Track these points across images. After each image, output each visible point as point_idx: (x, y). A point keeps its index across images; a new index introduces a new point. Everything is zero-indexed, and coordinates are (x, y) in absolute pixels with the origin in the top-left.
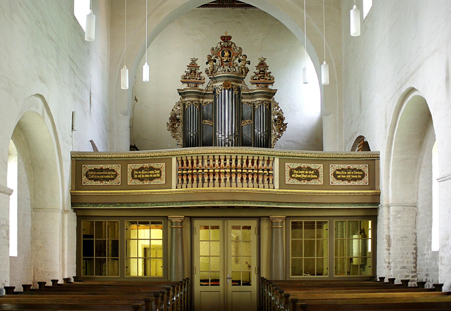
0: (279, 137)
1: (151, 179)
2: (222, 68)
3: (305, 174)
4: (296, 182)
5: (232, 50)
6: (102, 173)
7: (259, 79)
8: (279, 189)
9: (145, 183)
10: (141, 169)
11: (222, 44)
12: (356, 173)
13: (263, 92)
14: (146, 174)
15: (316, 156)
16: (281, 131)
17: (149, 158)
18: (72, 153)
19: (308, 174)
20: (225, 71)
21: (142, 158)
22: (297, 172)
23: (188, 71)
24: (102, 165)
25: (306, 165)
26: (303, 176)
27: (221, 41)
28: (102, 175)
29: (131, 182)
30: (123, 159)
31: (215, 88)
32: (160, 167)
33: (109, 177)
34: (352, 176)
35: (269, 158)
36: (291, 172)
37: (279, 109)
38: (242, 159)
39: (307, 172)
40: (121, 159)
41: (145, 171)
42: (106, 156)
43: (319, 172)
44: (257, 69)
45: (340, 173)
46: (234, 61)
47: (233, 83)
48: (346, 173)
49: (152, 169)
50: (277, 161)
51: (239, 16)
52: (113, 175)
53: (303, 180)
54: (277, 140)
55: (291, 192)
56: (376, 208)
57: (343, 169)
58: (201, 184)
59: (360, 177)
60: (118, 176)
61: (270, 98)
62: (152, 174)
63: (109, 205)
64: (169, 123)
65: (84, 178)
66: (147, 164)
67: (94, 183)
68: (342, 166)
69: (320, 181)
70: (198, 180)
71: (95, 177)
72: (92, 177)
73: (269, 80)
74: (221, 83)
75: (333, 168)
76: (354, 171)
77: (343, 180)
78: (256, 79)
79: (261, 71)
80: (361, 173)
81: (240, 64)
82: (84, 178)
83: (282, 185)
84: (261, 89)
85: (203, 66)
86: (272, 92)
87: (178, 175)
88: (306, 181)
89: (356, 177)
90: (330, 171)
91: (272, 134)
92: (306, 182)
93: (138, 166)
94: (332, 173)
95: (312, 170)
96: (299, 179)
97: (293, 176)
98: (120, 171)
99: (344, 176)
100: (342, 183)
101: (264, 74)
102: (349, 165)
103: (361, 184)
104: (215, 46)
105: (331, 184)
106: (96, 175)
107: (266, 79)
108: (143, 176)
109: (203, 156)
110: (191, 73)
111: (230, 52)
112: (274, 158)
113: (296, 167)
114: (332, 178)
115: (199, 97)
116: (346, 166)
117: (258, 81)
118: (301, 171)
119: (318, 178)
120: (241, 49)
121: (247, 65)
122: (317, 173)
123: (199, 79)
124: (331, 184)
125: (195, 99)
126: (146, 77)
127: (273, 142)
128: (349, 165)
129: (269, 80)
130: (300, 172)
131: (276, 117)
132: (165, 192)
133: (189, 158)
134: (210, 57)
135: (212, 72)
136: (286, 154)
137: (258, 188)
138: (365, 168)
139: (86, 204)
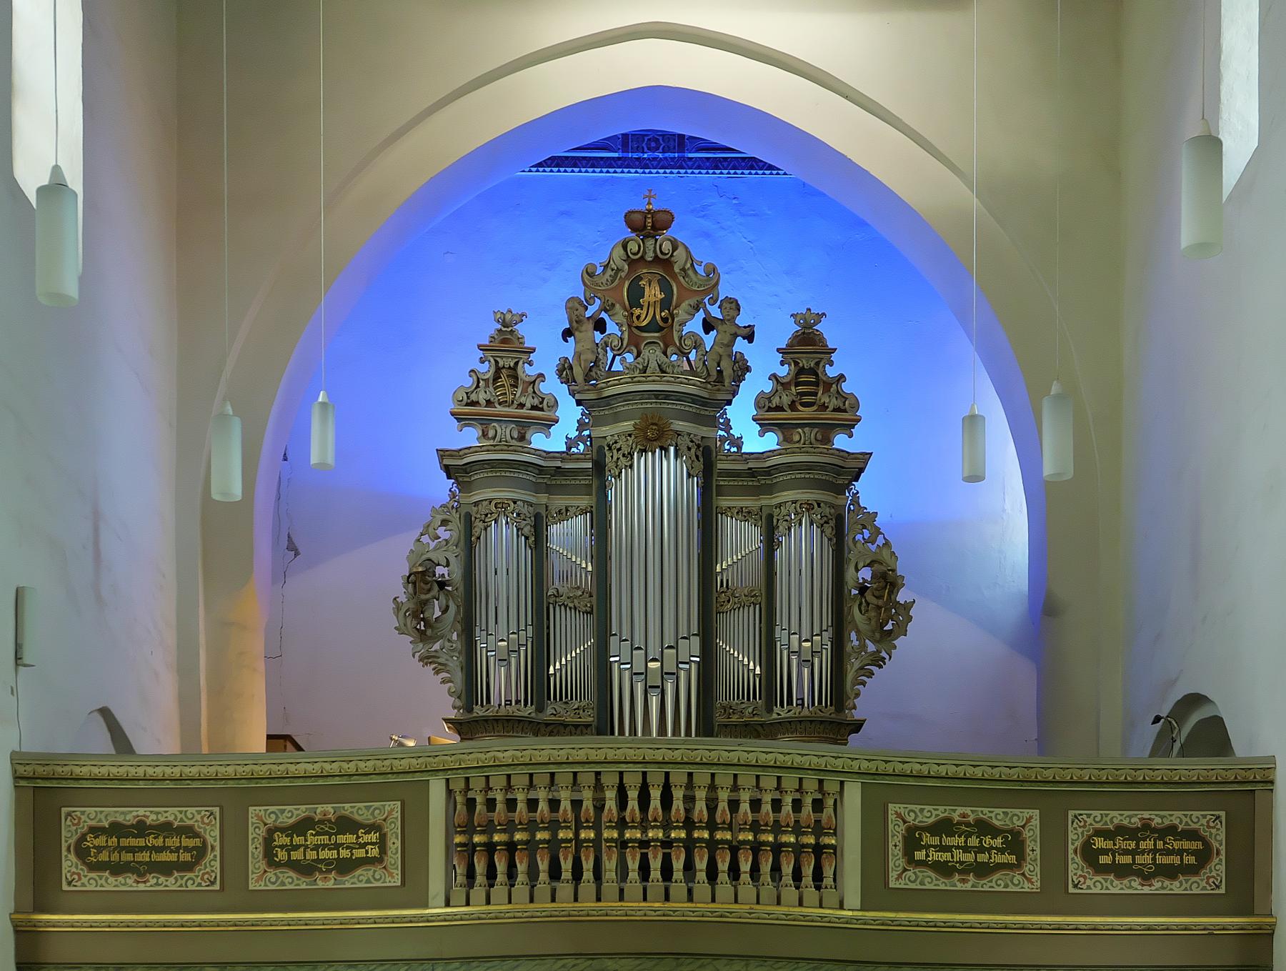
0: (878, 661)
1: (345, 867)
2: (630, 358)
3: (966, 849)
4: (932, 882)
5: (674, 276)
6: (141, 842)
7: (792, 406)
9: (321, 885)
10: (302, 826)
11: (633, 247)
12: (1177, 845)
13: (809, 466)
14: (324, 846)
16: (886, 638)
17: (336, 781)
18: (17, 759)
19: (981, 849)
22: (936, 841)
23: (483, 368)
24: (141, 811)
26: (959, 855)
27: (628, 233)
28: (141, 849)
29: (260, 879)
31: (601, 448)
32: (379, 818)
34: (1161, 860)
36: (912, 842)
37: (880, 541)
38: (713, 787)
39: (973, 841)
40: (220, 785)
41: (318, 834)
42: (158, 770)
43: (1023, 842)
44: (782, 363)
45: (1109, 844)
46: (683, 324)
47: (679, 425)
48: (1133, 845)
49: (346, 825)
51: (704, 208)
52: (187, 849)
54: (871, 674)
57: (1121, 831)
60: (210, 856)
61: (840, 490)
64: (403, 598)
65: (70, 863)
66: (329, 808)
67: (111, 883)
68: (1118, 817)
69: (1029, 880)
72: (104, 857)
74: (627, 426)
75: (1082, 824)
76: (1169, 838)
77: (1121, 872)
78: (779, 408)
79: (801, 371)
80: (1197, 845)
81: (709, 340)
82: (70, 863)
83: (876, 891)
84: (801, 451)
85: (547, 350)
86: (851, 464)
88: (971, 877)
89: (1176, 860)
90: (1071, 836)
91: (848, 648)
92: (971, 883)
93: (291, 814)
94: (1078, 844)
96: (944, 869)
97: (920, 855)
98: (217, 833)
99: (1127, 859)
100: (1116, 887)
102: (1146, 815)
103: (1195, 891)
104: (599, 259)
105: (1071, 890)
106: (120, 849)
107: (824, 407)
108: (311, 855)
110: (496, 377)
111: (665, 287)
112: (842, 783)
113: (931, 820)
114: (1076, 866)
115: (537, 488)
116: (1133, 819)
118: (951, 835)
119: (1018, 866)
122: (1015, 843)
123: (534, 408)
124: (1071, 890)
125: (515, 496)
126: (321, 447)
128: (1146, 815)
130: (948, 841)
131: (866, 574)
135: (587, 378)
136: (889, 768)
137: (779, 903)
138: (1211, 824)
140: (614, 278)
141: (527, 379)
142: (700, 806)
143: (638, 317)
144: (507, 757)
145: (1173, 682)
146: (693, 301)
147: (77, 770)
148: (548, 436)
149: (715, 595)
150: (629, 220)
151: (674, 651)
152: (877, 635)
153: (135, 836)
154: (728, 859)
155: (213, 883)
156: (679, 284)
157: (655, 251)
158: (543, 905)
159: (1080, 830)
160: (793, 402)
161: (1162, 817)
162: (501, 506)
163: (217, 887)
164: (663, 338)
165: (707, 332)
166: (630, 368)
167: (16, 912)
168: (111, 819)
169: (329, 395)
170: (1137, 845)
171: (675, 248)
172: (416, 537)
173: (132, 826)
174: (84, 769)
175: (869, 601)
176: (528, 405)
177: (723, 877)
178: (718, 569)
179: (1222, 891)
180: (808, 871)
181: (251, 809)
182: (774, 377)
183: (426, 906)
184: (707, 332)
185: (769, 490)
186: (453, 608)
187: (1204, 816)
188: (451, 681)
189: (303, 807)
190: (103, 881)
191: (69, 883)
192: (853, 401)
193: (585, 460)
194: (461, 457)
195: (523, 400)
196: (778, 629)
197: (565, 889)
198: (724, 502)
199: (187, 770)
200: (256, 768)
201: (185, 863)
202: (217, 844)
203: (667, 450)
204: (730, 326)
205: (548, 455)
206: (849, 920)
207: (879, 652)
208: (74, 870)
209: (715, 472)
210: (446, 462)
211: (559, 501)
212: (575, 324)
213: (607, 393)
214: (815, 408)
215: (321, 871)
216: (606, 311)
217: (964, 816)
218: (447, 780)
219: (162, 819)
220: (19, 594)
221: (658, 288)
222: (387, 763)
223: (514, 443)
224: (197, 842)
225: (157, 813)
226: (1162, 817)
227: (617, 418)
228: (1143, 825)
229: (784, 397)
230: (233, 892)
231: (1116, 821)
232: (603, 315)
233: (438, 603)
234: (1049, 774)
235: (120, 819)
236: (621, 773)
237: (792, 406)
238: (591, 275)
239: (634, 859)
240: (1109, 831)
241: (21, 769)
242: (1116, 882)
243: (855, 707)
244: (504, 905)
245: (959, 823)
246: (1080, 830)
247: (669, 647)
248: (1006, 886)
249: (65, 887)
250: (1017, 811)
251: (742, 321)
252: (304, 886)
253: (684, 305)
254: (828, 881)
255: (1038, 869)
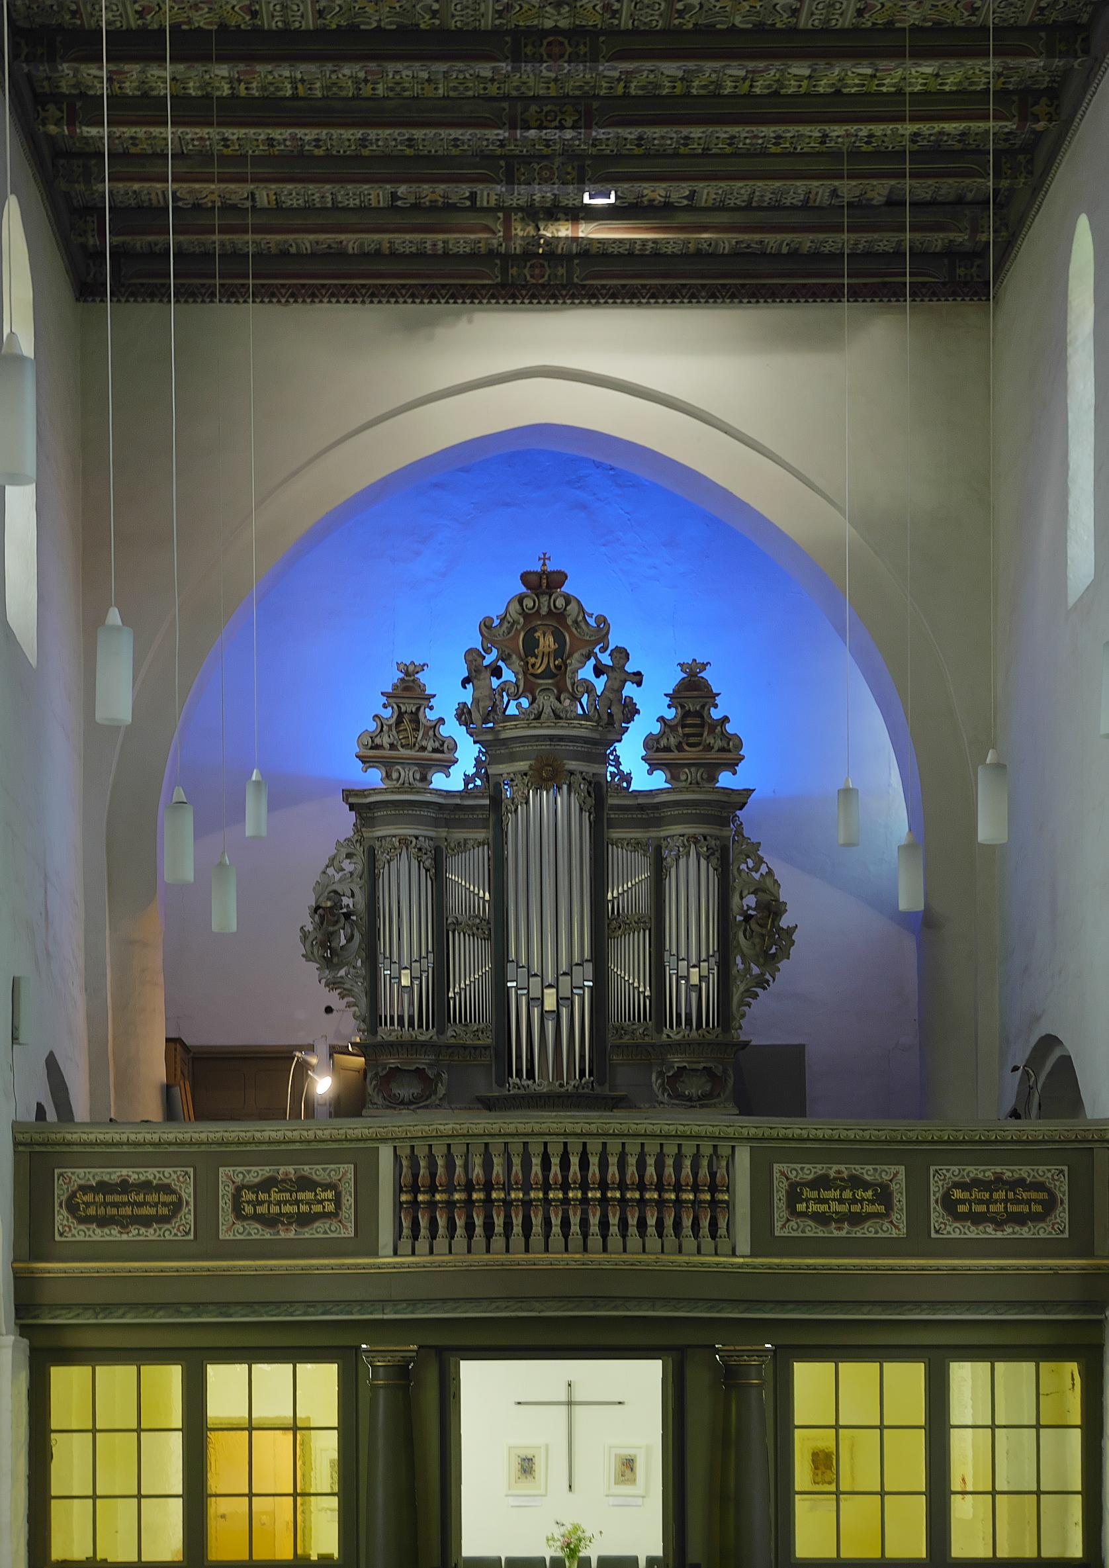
0: (762, 983)
1: (305, 1220)
2: (525, 703)
3: (841, 1201)
4: (813, 1230)
5: (567, 628)
7: (679, 748)
8: (751, 1256)
9: (283, 1235)
10: (267, 1184)
11: (528, 603)
14: (286, 1202)
15: (882, 1135)
17: (297, 1146)
19: (854, 1201)
20: (538, 717)
21: (273, 1147)
22: (815, 1194)
24: (124, 1172)
25: (845, 1170)
26: (835, 1206)
27: (523, 589)
28: (124, 1204)
29: (229, 1230)
30: (203, 1148)
32: (335, 1178)
33: (152, 1211)
34: (1010, 1208)
35: (715, 1147)
36: (794, 1195)
39: (847, 1194)
40: (194, 1149)
41: (280, 1191)
44: (669, 706)
45: (966, 1195)
47: (572, 765)
49: (305, 1183)
50: (743, 1157)
52: (164, 1204)
53: (836, 1221)
54: (749, 1005)
55: (793, 1267)
56: (1100, 1322)
57: (976, 1183)
58: (483, 1241)
59: (1039, 1208)
60: (185, 1210)
61: (724, 822)
62: (309, 1203)
63: (152, 1311)
64: (310, 928)
65: (61, 1217)
66: (291, 1169)
67: (98, 1234)
68: (973, 1172)
69: (897, 1227)
70: (470, 1227)
71: (101, 1211)
72: (91, 1211)
73: (722, 750)
74: (523, 765)
75: (941, 1177)
77: (977, 1219)
78: (667, 749)
80: (1043, 1196)
81: (600, 684)
83: (763, 1241)
84: (687, 790)
85: (447, 696)
86: (736, 799)
87: (398, 1206)
91: (734, 972)
94: (939, 1195)
95: (866, 1186)
96: (822, 1219)
97: (801, 1207)
99: (982, 1208)
100: (973, 1232)
101: (702, 726)
102: (998, 1169)
105: (933, 1235)
106: (105, 1204)
107: (709, 748)
108: (275, 1209)
109: (486, 1144)
110: (399, 722)
111: (559, 638)
112: (733, 1147)
113: (810, 1177)
114: (937, 1215)
115: (436, 823)
116: (987, 1172)
117: (676, 754)
119: (887, 1215)
120: (605, 621)
121: (629, 690)
122: (884, 1195)
123: (435, 750)
125: (416, 832)
127: (740, 1006)
128: (998, 1169)
129: (722, 750)
131: (751, 900)
132: (357, 1266)
133: (439, 1151)
134: (473, 657)
139: (68, 1307)
140: (510, 630)
141: (428, 724)
142: (613, 1170)
143: (533, 665)
144: (447, 1129)
145: (1038, 1018)
146: (585, 651)
147: (69, 1137)
148: (448, 776)
149: (607, 921)
150: (525, 578)
151: (569, 978)
152: (761, 960)
153: (119, 1193)
154: (637, 1215)
155: (187, 1233)
156: (571, 633)
157: (549, 606)
158: (480, 1258)
159: (940, 1183)
160: (680, 743)
161: (1012, 1171)
162: (404, 841)
163: (191, 1237)
164: (556, 685)
165: (597, 676)
166: (524, 712)
167: (15, 1260)
168: (98, 1178)
169: (262, 773)
170: (991, 1196)
171: (568, 602)
172: (321, 870)
173: (116, 1184)
174: (75, 1136)
175: (754, 931)
176: (430, 749)
177: (633, 1230)
178: (610, 897)
179: (1066, 1235)
180: (705, 1223)
181: (221, 1169)
182: (661, 719)
183: (376, 1254)
184: (597, 676)
185: (658, 822)
186: (357, 937)
187: (1049, 1171)
188: (355, 1005)
189: (267, 1168)
190: (91, 1233)
191: (61, 1235)
192: (737, 741)
193: (483, 797)
194: (366, 796)
195: (424, 743)
196: (667, 954)
197: (498, 1242)
198: (615, 834)
199: (165, 1136)
200: (226, 1134)
201: (163, 1216)
202: (191, 1200)
203: (559, 788)
204: (619, 671)
205: (449, 794)
206: (741, 1266)
207: (763, 974)
208: (65, 1222)
209: (605, 805)
210: (351, 800)
211: (459, 835)
212: (474, 674)
213: (503, 735)
214: (701, 747)
215: (283, 1224)
216: (503, 660)
217: (839, 1172)
218: (395, 1147)
219: (143, 1178)
220: (15, 983)
221: (552, 639)
222: (341, 1132)
223: (419, 785)
224: (174, 1198)
225: (138, 1173)
226: (1012, 1171)
227: (512, 758)
228: (996, 1179)
229: (672, 739)
230: (206, 1243)
231: (972, 1175)
232: (500, 663)
233: (342, 933)
234: (912, 1135)
235: (106, 1178)
236: (546, 1144)
237: (679, 748)
238: (489, 627)
239: (556, 1216)
240: (966, 1183)
241: (20, 1137)
242: (972, 1228)
243: (741, 1028)
244: (445, 1257)
245: (835, 1179)
246: (940, 1183)
247: (565, 974)
248: (876, 1232)
249: (57, 1238)
250: (885, 1167)
251: (630, 667)
252: (268, 1236)
253: (576, 656)
254: (722, 1231)
255: (904, 1218)
